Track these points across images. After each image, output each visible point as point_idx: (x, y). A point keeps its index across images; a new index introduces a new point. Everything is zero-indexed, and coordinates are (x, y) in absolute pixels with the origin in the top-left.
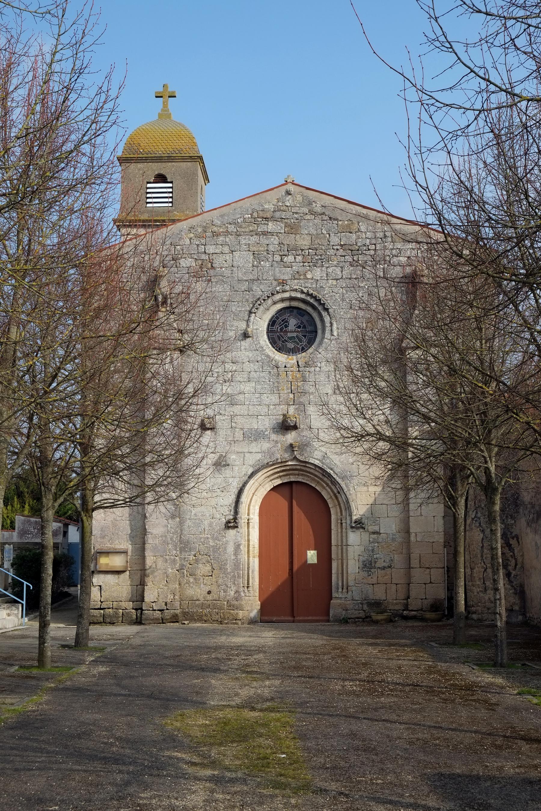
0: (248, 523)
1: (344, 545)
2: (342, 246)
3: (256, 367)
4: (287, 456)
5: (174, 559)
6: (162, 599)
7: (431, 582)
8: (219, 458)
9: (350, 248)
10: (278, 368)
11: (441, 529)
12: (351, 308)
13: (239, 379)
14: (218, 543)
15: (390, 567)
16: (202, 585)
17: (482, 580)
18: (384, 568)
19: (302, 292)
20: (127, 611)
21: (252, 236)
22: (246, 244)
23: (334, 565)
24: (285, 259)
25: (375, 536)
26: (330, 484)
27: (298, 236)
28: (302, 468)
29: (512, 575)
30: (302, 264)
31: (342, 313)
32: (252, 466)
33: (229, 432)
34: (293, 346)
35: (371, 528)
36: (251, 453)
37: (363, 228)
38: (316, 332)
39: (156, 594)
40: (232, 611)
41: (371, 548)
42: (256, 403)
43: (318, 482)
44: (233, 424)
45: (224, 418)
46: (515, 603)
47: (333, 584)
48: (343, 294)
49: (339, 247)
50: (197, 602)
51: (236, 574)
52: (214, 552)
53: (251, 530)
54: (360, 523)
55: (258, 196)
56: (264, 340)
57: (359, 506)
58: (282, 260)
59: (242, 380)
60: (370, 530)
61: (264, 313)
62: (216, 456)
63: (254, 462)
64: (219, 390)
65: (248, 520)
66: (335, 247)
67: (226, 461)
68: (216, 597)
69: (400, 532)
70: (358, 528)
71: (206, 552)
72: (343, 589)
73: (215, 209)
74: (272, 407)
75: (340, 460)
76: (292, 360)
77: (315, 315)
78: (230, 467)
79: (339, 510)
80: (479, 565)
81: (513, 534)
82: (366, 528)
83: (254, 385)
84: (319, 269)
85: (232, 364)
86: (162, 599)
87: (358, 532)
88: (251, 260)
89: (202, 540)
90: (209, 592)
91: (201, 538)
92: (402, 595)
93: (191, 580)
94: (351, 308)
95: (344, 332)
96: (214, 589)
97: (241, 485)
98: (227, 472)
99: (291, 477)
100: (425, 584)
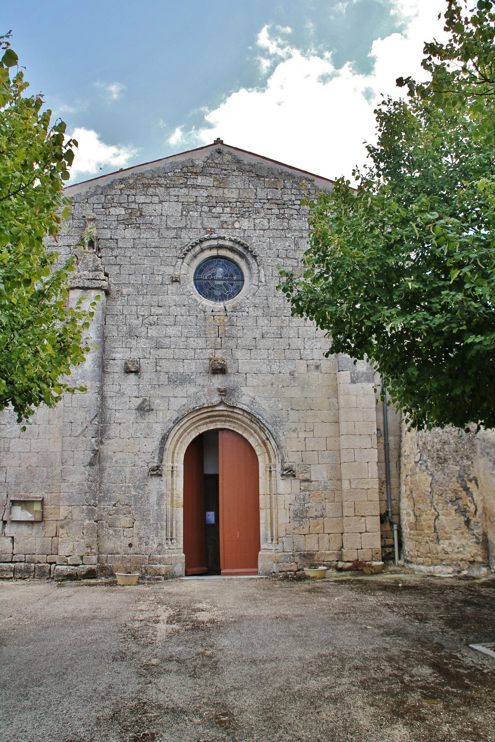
0: (172, 471)
1: (273, 494)
2: (268, 200)
3: (183, 311)
4: (216, 399)
5: (92, 510)
6: (78, 552)
7: (366, 531)
8: (143, 402)
9: (277, 202)
10: (205, 312)
11: (376, 475)
12: (278, 256)
13: (165, 322)
14: (141, 492)
15: (322, 516)
16: (122, 538)
17: (433, 529)
18: (316, 517)
19: (230, 240)
20: (40, 565)
21: (181, 188)
22: (175, 196)
23: (263, 515)
24: (214, 211)
25: (306, 484)
26: (259, 431)
27: (227, 189)
28: (230, 414)
29: (472, 522)
30: (230, 215)
31: (269, 261)
32: (178, 411)
33: (153, 375)
34: (220, 294)
35: (301, 476)
36: (176, 397)
37: (288, 185)
38: (243, 280)
39: (70, 547)
40: (154, 566)
41: (302, 497)
42: (182, 347)
43: (246, 429)
44: (158, 368)
45: (148, 361)
46: (477, 553)
47: (261, 535)
48: (270, 243)
49: (265, 201)
50: (117, 556)
51: (159, 526)
52: (135, 501)
53: (174, 478)
54: (290, 471)
55: (188, 154)
56: (191, 286)
57: (289, 453)
58: (210, 211)
59: (168, 324)
60: (301, 478)
61: (192, 260)
62: (139, 401)
63: (179, 407)
64: (144, 333)
65: (172, 468)
66: (262, 201)
67: (150, 406)
68: (137, 550)
69: (331, 480)
70: (287, 476)
71: (126, 502)
72: (272, 540)
73: (147, 164)
74: (198, 351)
75: (269, 405)
76: (220, 305)
77: (242, 264)
78: (154, 412)
79: (267, 458)
80: (428, 512)
81: (471, 477)
82: (297, 476)
83: (180, 328)
84: (246, 220)
85: (158, 308)
86: (78, 552)
87: (289, 481)
88: (180, 210)
89: (123, 489)
90: (130, 545)
91: (122, 487)
92: (335, 546)
93: (111, 532)
94: (278, 256)
95: (272, 279)
96: (135, 541)
97: (165, 431)
98: (151, 417)
99: (218, 423)
100: (360, 533)
